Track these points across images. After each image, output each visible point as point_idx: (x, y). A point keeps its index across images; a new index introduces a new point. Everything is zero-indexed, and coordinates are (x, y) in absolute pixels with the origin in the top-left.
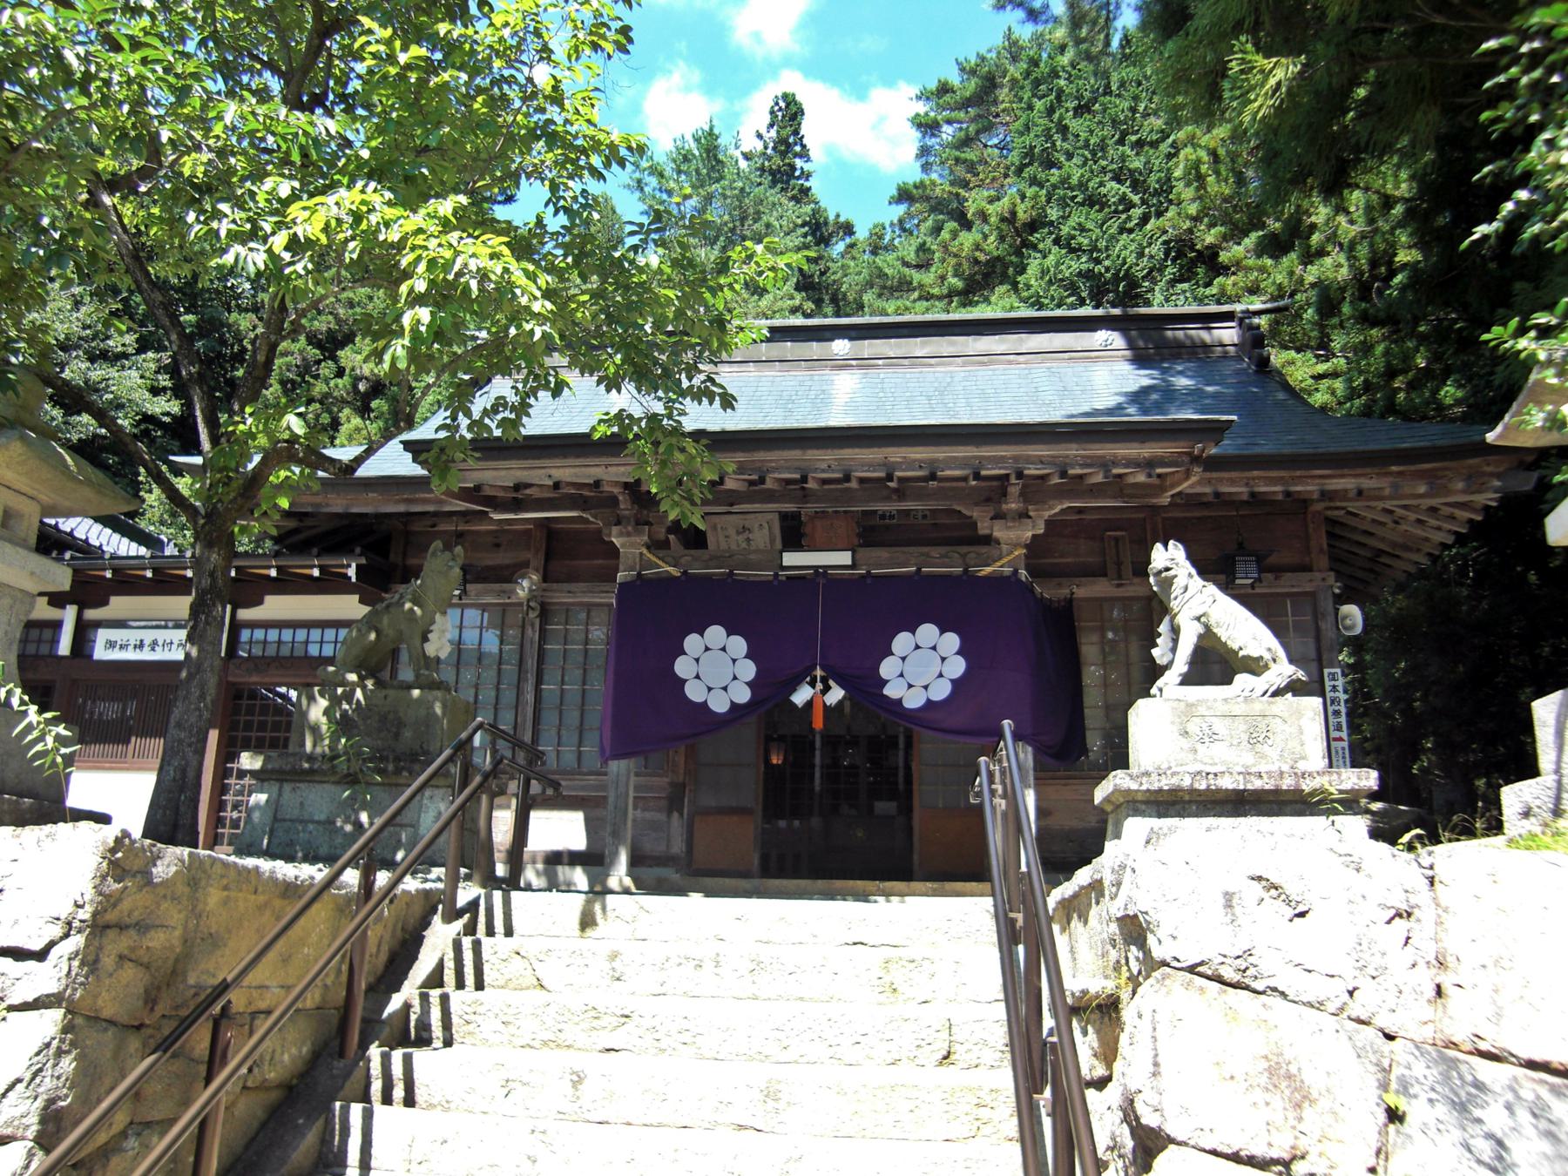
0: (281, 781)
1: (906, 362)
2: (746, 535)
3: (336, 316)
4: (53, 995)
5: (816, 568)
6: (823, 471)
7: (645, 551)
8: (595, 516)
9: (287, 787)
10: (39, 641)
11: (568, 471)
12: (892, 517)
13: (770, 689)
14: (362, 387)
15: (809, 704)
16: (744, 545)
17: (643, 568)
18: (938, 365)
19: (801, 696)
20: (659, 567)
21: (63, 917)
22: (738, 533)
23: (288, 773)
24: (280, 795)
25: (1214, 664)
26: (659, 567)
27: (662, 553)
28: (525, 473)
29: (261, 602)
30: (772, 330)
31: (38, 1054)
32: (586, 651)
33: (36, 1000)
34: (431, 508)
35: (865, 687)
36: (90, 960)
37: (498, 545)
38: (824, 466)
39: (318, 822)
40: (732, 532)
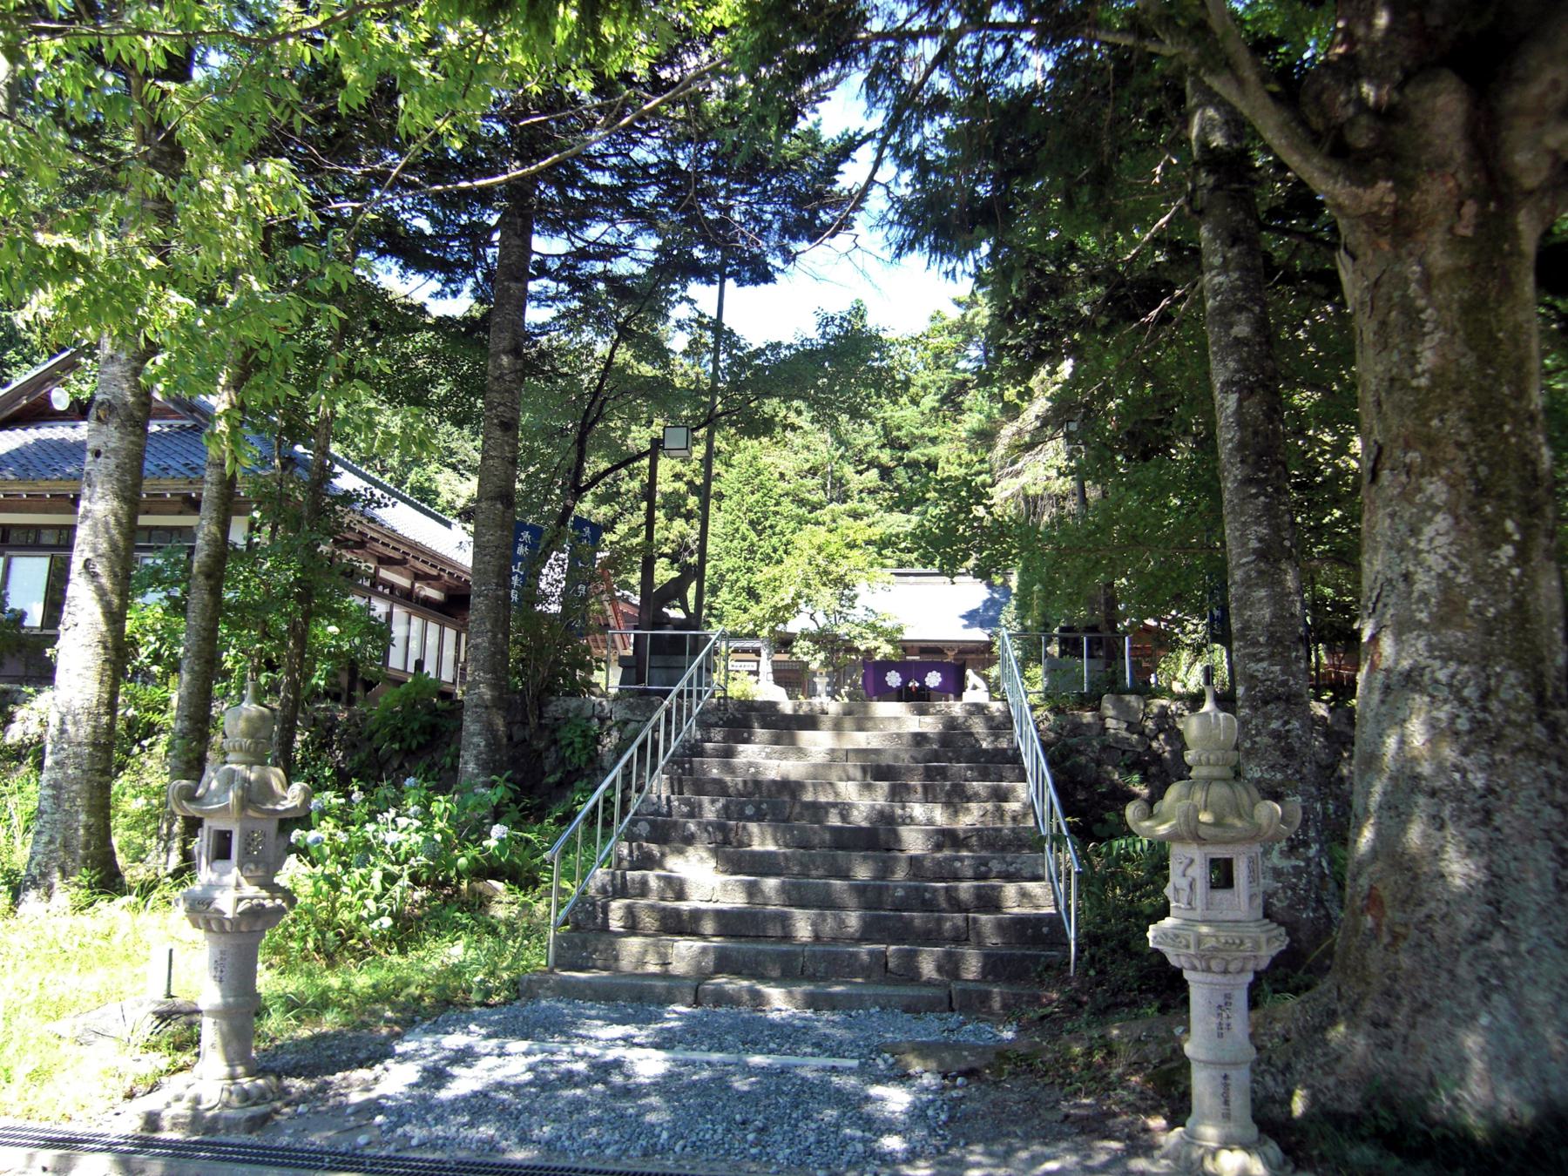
13: (905, 682)
25: (975, 688)
35: (923, 683)
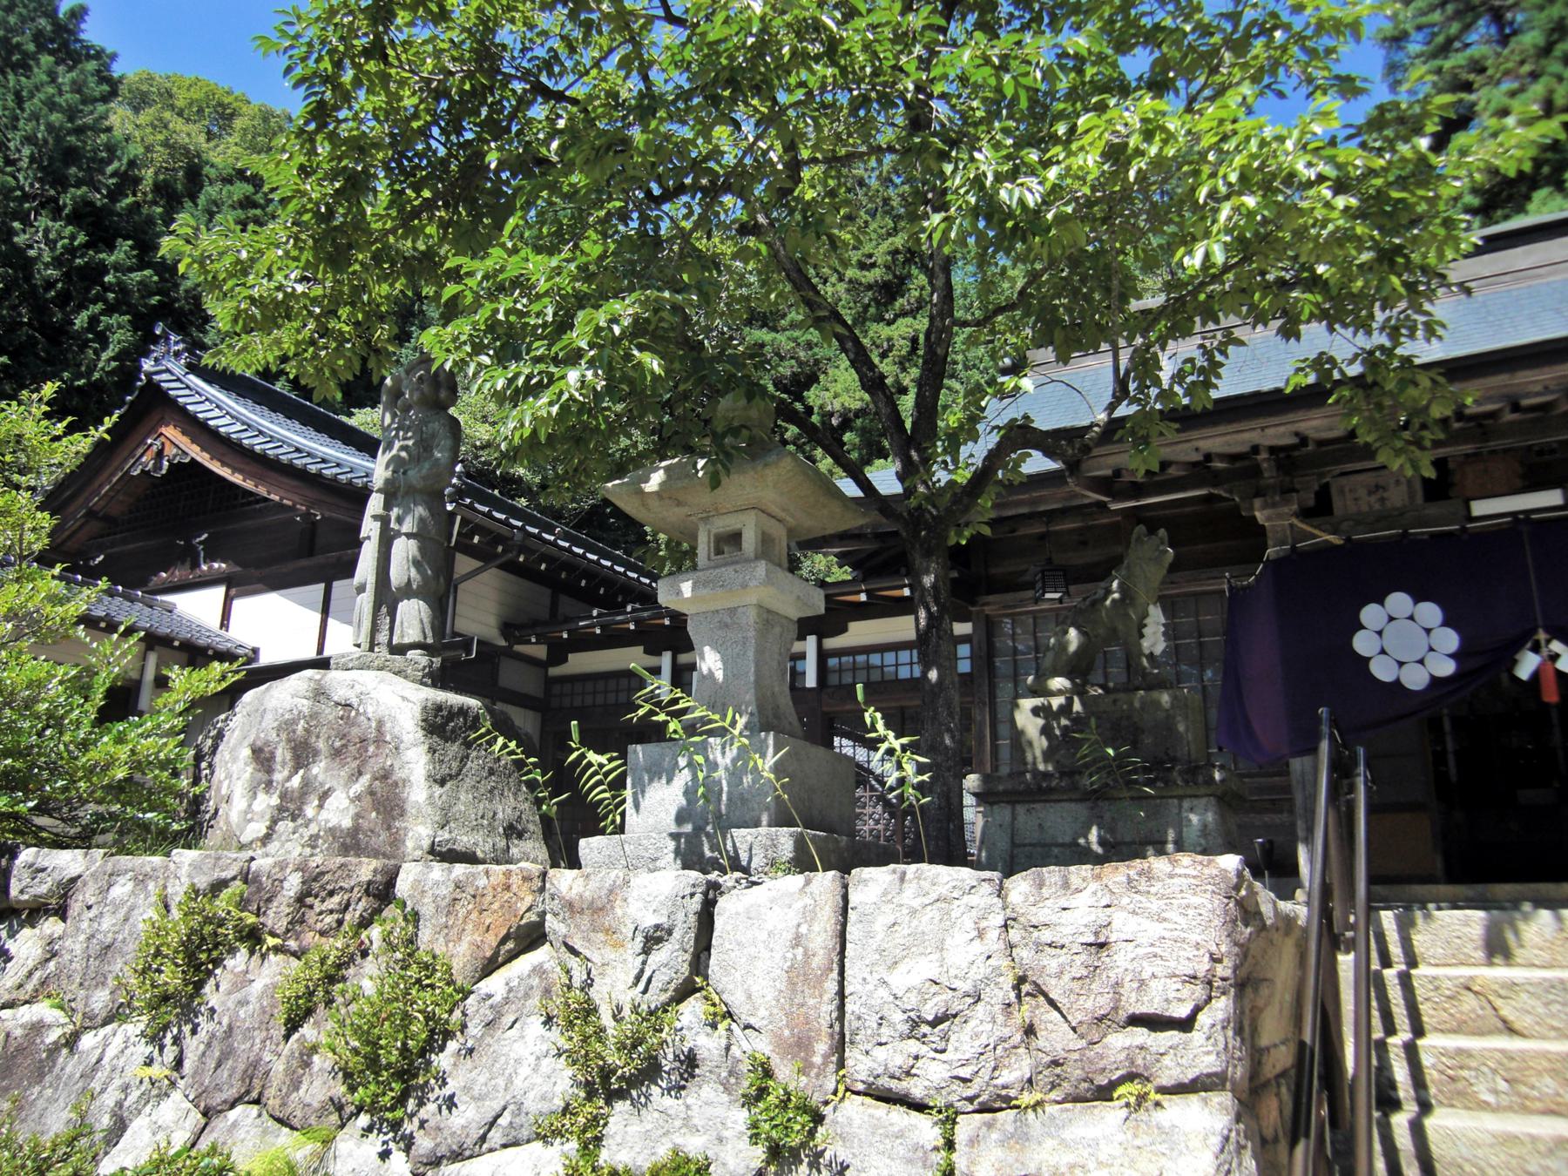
0: (1013, 803)
1: (1507, 278)
2: (1380, 493)
3: (797, 359)
4: (1215, 1074)
5: (1514, 514)
6: (1538, 394)
7: (1295, 521)
8: (1231, 492)
9: (1020, 809)
10: (595, 693)
11: (1218, 440)
12: (1552, 451)
13: (1484, 658)
14: (835, 422)
15: (1536, 675)
16: (1377, 506)
17: (1296, 541)
18: (1550, 274)
19: (1528, 664)
20: (1315, 537)
21: (1201, 974)
22: (1370, 493)
23: (1020, 793)
24: (1014, 818)
26: (1315, 537)
27: (1317, 521)
28: (1168, 450)
29: (844, 630)
30: (1487, 239)
31: (1222, 1151)
32: (1015, 661)
33: (1194, 1081)
34: (1024, 510)
36: (1244, 1025)
37: (1084, 543)
38: (1538, 388)
39: (1062, 845)
40: (1362, 492)
